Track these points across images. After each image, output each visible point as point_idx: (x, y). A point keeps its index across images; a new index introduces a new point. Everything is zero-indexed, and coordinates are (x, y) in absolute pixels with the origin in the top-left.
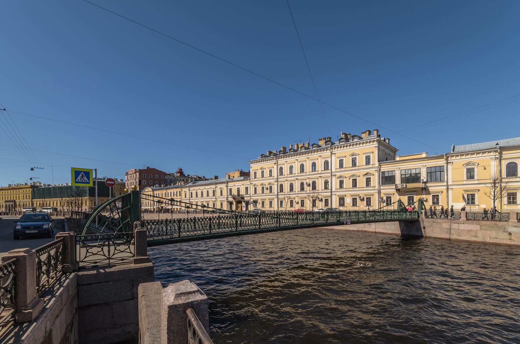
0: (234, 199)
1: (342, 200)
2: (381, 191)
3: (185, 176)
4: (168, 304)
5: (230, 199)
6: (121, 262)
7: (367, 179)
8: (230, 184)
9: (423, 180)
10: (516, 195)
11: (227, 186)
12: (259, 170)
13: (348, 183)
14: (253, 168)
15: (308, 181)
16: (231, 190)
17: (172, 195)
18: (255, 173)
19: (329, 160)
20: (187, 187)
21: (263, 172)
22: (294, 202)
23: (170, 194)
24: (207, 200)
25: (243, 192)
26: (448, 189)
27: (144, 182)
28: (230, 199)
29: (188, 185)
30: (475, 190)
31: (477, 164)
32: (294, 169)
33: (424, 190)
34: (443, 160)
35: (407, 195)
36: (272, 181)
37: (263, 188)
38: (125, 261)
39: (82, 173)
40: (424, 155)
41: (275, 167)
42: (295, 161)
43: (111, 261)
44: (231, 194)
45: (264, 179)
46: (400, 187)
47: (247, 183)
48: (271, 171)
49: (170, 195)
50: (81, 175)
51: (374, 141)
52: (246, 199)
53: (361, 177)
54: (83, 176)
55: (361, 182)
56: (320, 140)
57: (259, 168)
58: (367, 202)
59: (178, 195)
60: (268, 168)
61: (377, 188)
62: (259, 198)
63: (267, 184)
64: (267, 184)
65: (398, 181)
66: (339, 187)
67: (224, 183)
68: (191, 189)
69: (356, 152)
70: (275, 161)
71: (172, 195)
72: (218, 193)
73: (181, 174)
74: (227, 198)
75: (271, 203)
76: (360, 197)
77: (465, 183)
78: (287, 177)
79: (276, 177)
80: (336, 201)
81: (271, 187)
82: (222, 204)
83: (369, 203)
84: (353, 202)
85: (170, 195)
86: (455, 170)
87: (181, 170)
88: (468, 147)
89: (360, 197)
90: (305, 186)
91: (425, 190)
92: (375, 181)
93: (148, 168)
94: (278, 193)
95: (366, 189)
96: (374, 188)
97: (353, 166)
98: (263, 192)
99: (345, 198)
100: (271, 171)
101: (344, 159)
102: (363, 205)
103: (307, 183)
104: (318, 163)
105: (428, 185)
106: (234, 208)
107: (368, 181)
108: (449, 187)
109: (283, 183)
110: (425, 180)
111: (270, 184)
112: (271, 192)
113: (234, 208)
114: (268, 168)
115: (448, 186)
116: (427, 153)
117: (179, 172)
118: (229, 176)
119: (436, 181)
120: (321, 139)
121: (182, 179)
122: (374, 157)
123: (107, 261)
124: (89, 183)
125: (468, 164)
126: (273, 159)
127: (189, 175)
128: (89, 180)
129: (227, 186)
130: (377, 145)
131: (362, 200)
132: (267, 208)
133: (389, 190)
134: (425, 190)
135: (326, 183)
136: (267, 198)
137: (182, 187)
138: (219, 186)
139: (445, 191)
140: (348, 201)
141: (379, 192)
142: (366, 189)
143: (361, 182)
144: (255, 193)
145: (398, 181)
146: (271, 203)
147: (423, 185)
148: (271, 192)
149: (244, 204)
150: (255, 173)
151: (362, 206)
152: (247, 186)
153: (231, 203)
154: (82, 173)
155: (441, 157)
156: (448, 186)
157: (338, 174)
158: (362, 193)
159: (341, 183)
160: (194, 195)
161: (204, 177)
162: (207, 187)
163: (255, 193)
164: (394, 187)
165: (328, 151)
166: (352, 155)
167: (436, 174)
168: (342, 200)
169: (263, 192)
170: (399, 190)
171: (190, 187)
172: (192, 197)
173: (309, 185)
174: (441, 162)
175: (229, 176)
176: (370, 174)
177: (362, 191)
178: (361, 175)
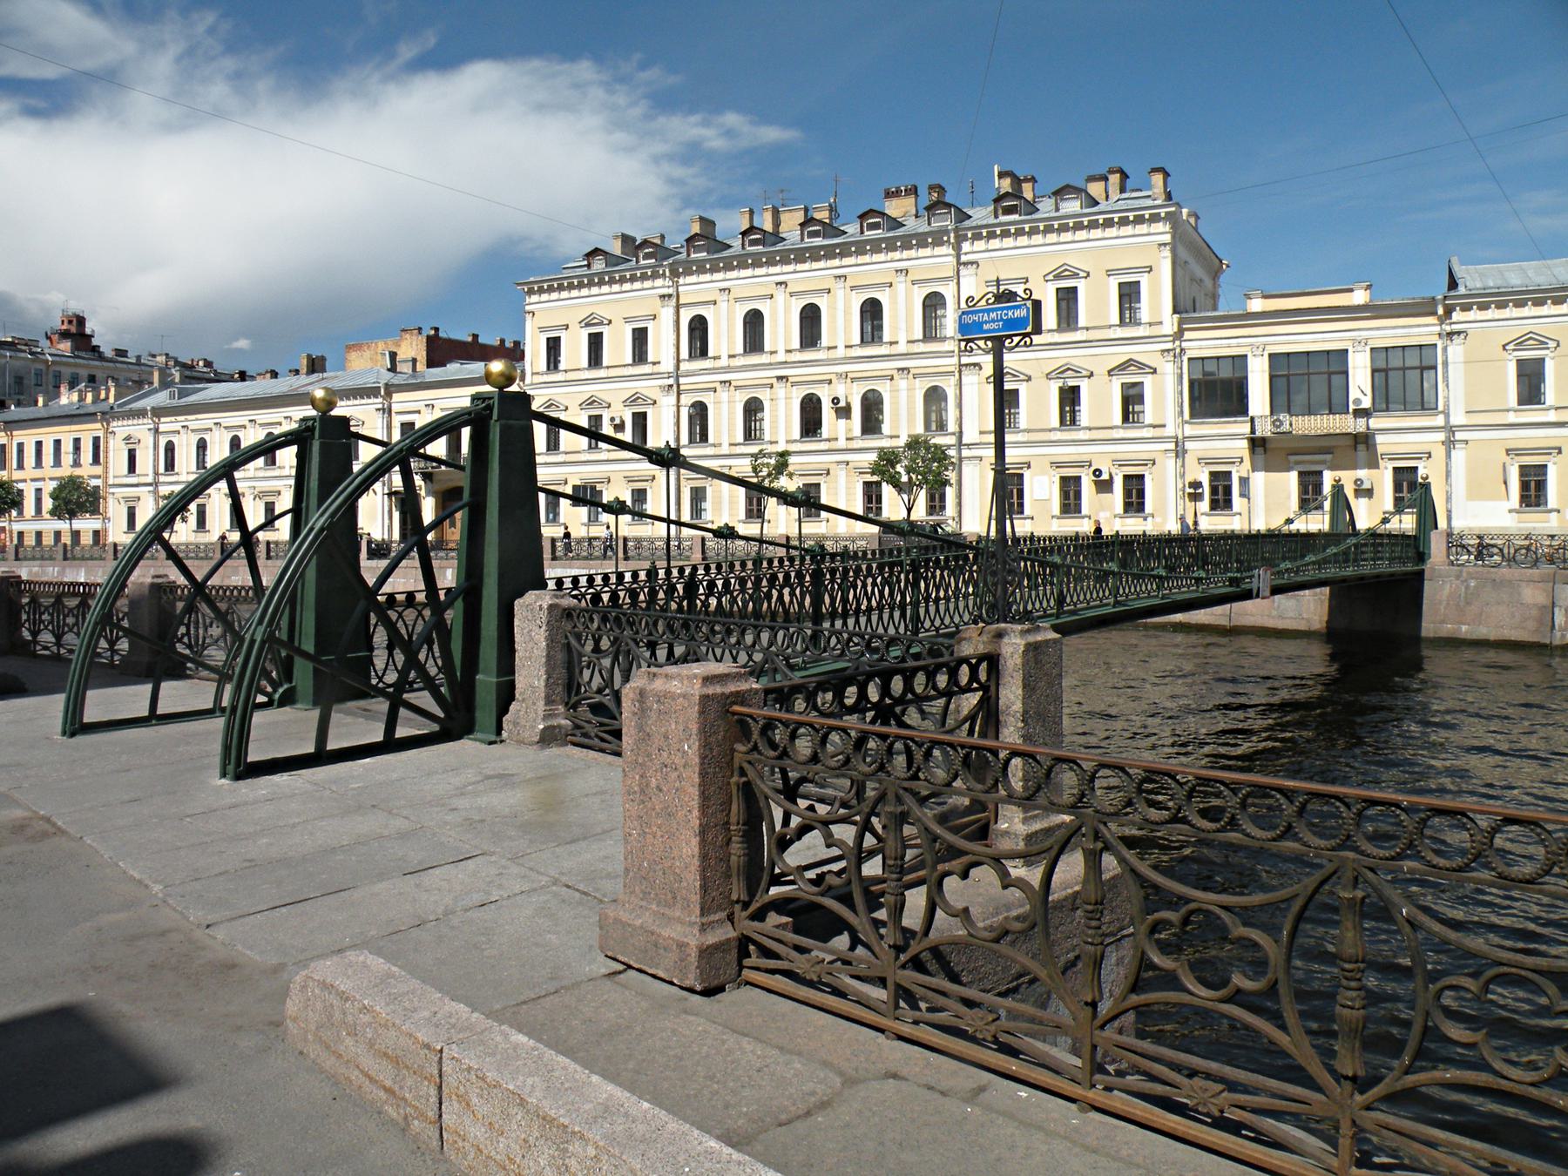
2: (1188, 445)
10: (1545, 474)
11: (387, 411)
12: (574, 327)
14: (543, 319)
15: (840, 390)
18: (554, 346)
20: (141, 413)
21: (596, 342)
26: (1450, 444)
29: (148, 403)
30: (1547, 451)
31: (1552, 344)
33: (1361, 447)
34: (1431, 320)
35: (1298, 463)
36: (649, 388)
40: (1360, 297)
41: (667, 313)
42: (772, 289)
45: (601, 373)
46: (1265, 429)
48: (640, 337)
51: (1155, 218)
53: (1039, 381)
56: (889, 195)
58: (1127, 493)
60: (627, 320)
67: (371, 392)
68: (167, 424)
69: (1075, 262)
70: (662, 285)
73: (75, 348)
76: (1098, 473)
77: (1512, 418)
78: (728, 370)
79: (668, 365)
84: (1065, 494)
86: (1474, 366)
87: (81, 321)
88: (1515, 275)
89: (1098, 473)
90: (827, 413)
91: (1361, 447)
92: (1165, 396)
94: (156, 474)
95: (1121, 434)
97: (1122, 323)
99: (1027, 475)
100: (640, 337)
102: (1112, 507)
105: (1374, 423)
107: (1132, 399)
109: (707, 399)
110: (1366, 403)
111: (634, 400)
114: (627, 320)
116: (1369, 287)
117: (65, 335)
118: (393, 355)
119: (1406, 406)
120: (897, 194)
121: (84, 373)
122: (1155, 293)
125: (1520, 344)
126: (655, 276)
127: (121, 353)
129: (387, 411)
130: (1167, 238)
131: (1104, 486)
133: (1225, 440)
134: (1361, 447)
137: (108, 416)
140: (1041, 490)
141: (1180, 452)
142: (1121, 434)
147: (1360, 425)
150: (554, 346)
151: (1105, 514)
155: (1424, 308)
158: (1104, 458)
159: (1070, 397)
161: (208, 364)
164: (1246, 429)
165: (944, 250)
166: (1058, 277)
167: (1406, 381)
168: (1007, 491)
170: (1264, 440)
171: (159, 412)
173: (844, 412)
174: (1421, 330)
175: (393, 355)
176: (1141, 366)
177: (1102, 444)
178: (1100, 369)
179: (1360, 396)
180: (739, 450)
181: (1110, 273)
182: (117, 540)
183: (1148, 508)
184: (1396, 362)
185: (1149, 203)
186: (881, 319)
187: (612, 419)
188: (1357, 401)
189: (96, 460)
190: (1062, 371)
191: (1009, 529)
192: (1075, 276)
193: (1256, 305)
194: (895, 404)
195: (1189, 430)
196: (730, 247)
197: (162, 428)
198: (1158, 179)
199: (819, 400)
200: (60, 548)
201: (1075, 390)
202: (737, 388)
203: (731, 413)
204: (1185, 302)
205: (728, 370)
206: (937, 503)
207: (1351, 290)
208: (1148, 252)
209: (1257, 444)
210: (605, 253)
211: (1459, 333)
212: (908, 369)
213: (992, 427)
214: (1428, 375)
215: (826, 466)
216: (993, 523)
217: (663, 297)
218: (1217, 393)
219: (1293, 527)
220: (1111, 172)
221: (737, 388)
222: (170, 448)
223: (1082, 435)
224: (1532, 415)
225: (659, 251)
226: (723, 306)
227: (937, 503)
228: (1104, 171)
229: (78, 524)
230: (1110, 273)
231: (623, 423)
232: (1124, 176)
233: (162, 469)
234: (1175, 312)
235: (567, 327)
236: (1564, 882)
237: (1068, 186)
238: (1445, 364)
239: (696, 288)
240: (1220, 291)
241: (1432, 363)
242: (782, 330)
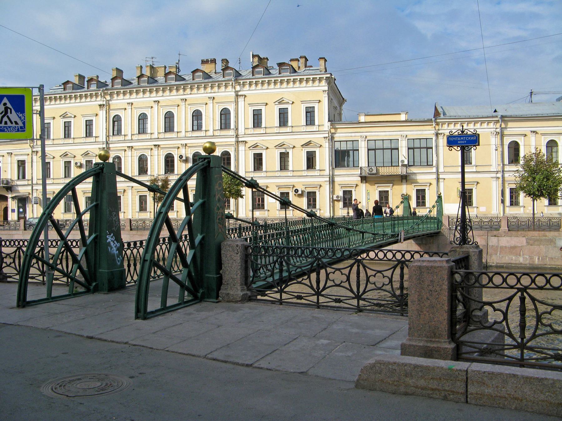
7: (281, 154)
15: (182, 152)
40: (403, 117)
45: (70, 141)
48: (89, 125)
55: (298, 160)
60: (83, 116)
76: (297, 191)
78: (186, 138)
79: (103, 138)
92: (324, 159)
96: (322, 173)
100: (89, 125)
103: (181, 157)
105: (414, 170)
114: (83, 116)
130: (326, 88)
133: (347, 177)
139: (434, 182)
141: (332, 182)
157: (251, 140)
166: (280, 103)
178: (298, 145)
179: (404, 159)
181: (302, 102)
182: (59, 218)
184: (417, 145)
185: (318, 72)
186: (201, 120)
187: (76, 164)
188: (403, 161)
190: (281, 145)
191: (467, 213)
193: (362, 119)
196: (131, 83)
198: (322, 62)
199: (230, 154)
201: (260, 155)
202: (543, 134)
204: (332, 118)
206: (421, 201)
207: (400, 114)
208: (317, 93)
209: (364, 179)
212: (159, 146)
213: (460, 164)
214: (429, 150)
216: (460, 209)
217: (100, 105)
218: (341, 158)
220: (301, 57)
223: (289, 174)
224: (311, 173)
225: (102, 85)
226: (210, 105)
228: (298, 57)
232: (306, 60)
234: (329, 121)
235: (54, 118)
236: (559, 363)
237: (197, 69)
238: (437, 146)
239: (119, 102)
240: (342, 112)
241: (430, 146)
242: (155, 124)
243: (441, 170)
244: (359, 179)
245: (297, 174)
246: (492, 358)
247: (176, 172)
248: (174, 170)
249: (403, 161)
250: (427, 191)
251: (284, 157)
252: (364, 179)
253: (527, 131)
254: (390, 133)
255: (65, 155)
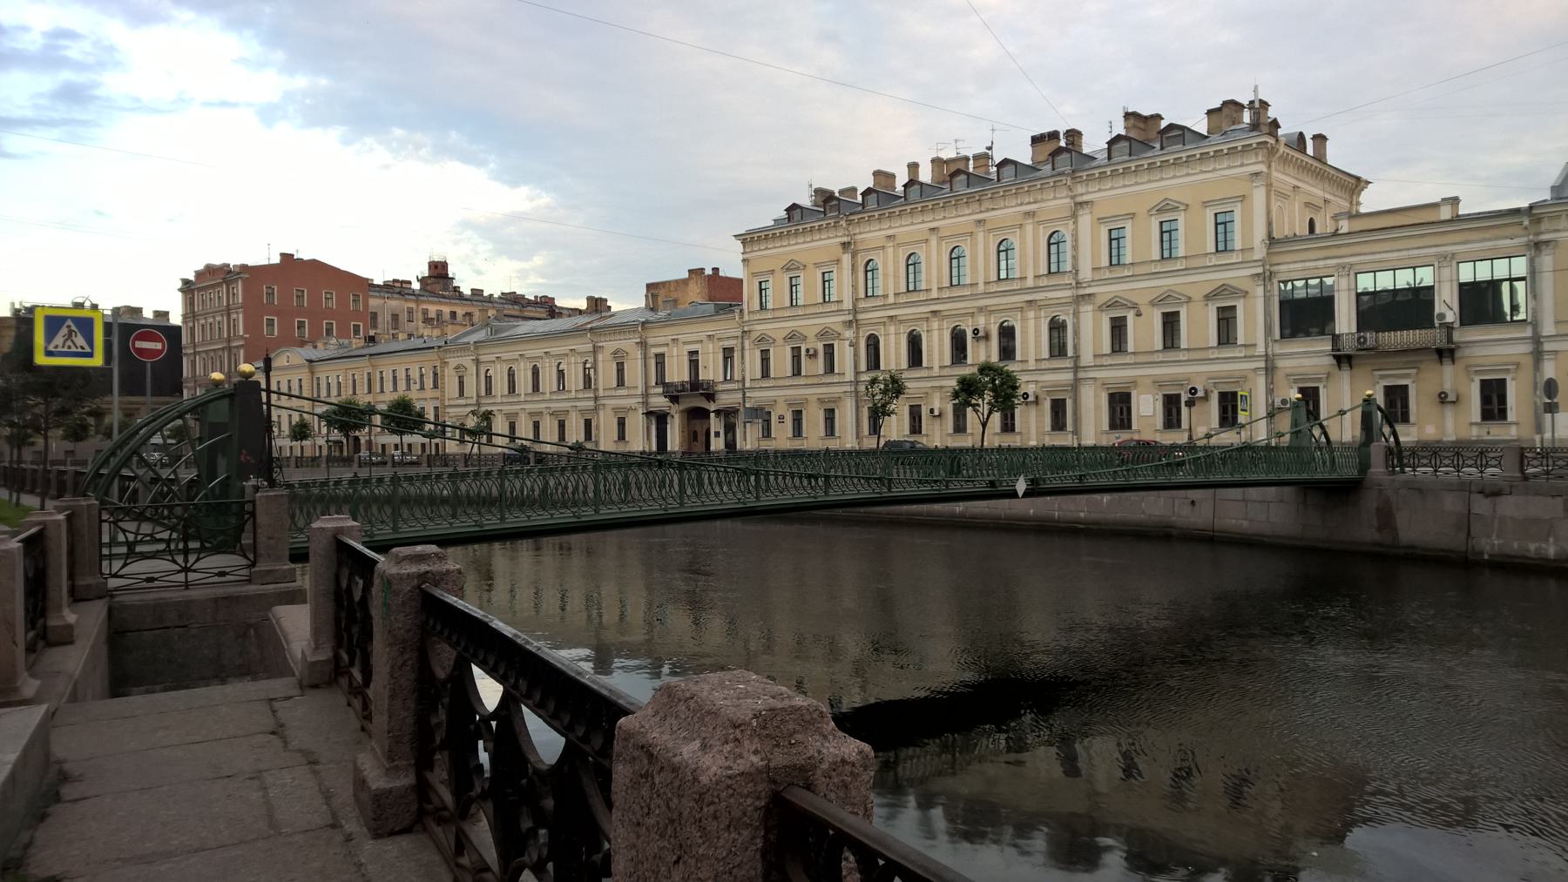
0: (674, 399)
1: (1120, 406)
2: (1280, 363)
3: (461, 296)
4: (308, 567)
5: (659, 402)
6: (216, 579)
7: (1165, 315)
8: (659, 339)
9: (1442, 316)
11: (643, 345)
13: (1145, 332)
15: (981, 322)
16: (660, 359)
17: (402, 385)
19: (1066, 232)
22: (925, 412)
23: (388, 377)
24: (506, 408)
25: (711, 371)
27: (270, 323)
28: (659, 402)
32: (966, 262)
35: (1382, 377)
36: (834, 322)
37: (796, 354)
38: (228, 578)
39: (69, 322)
43: (192, 576)
44: (661, 381)
47: (727, 329)
49: (389, 386)
50: (64, 331)
52: (725, 400)
54: (70, 332)
55: (1199, 326)
57: (777, 265)
59: (429, 382)
61: (1261, 350)
62: (777, 396)
63: (811, 333)
64: (811, 333)
65: (1345, 320)
66: (1107, 349)
71: (402, 385)
72: (606, 375)
74: (646, 395)
75: (830, 416)
77: (1156, 358)
80: (1097, 408)
81: (829, 350)
82: (536, 426)
83: (1228, 417)
85: (389, 386)
92: (1255, 320)
93: (286, 257)
94: (647, 387)
95: (1161, 357)
96: (1250, 352)
98: (797, 371)
101: (1128, 225)
103: (976, 332)
104: (928, 257)
106: (674, 442)
107: (1226, 319)
108: (1547, 347)
111: (822, 335)
112: (830, 368)
113: (674, 442)
115: (1537, 340)
123: (181, 577)
124: (91, 355)
128: (92, 346)
132: (814, 438)
135: (1057, 327)
136: (811, 393)
138: (610, 345)
139: (1528, 362)
141: (1270, 369)
143: (1199, 326)
144: (765, 373)
145: (1345, 320)
146: (830, 416)
148: (830, 368)
149: (715, 424)
152: (727, 344)
153: (661, 419)
154: (69, 322)
156: (1537, 340)
157: (1105, 292)
160: (500, 386)
162: (558, 348)
163: (765, 373)
168: (1120, 406)
169: (797, 371)
172: (489, 390)
177: (1202, 367)
178: (1198, 294)
179: (1444, 309)
180: (945, 372)
181: (1206, 204)
183: (1412, 419)
189: (436, 387)
192: (1175, 209)
194: (1025, 332)
195: (1278, 349)
197: (651, 341)
200: (425, 459)
203: (1038, 330)
205: (1036, 289)
206: (1495, 406)
209: (1343, 360)
210: (1015, 163)
211: (1547, 242)
215: (1514, 359)
217: (844, 244)
219: (1213, 441)
221: (901, 322)
222: (488, 379)
223: (1182, 356)
227: (1495, 406)
229: (407, 439)
230: (1206, 204)
231: (816, 351)
233: (483, 393)
235: (1132, 216)
243: (601, 393)
244: (1330, 361)
245: (1199, 354)
246: (269, 579)
247: (969, 361)
248: (1014, 350)
249: (1442, 316)
250: (1322, 393)
251: (1171, 322)
252: (1343, 360)
253: (702, 336)
254: (1377, 257)
255: (792, 336)
